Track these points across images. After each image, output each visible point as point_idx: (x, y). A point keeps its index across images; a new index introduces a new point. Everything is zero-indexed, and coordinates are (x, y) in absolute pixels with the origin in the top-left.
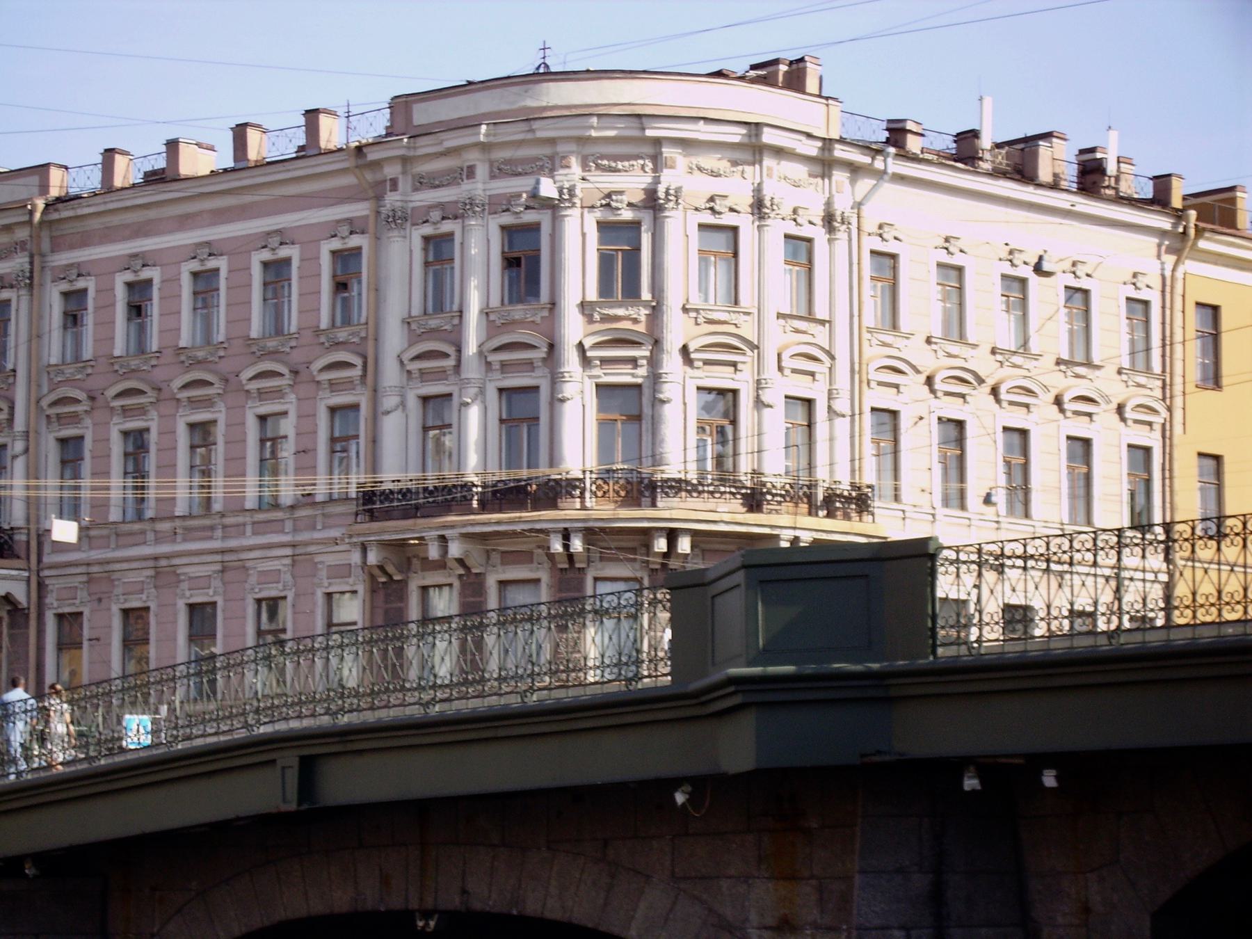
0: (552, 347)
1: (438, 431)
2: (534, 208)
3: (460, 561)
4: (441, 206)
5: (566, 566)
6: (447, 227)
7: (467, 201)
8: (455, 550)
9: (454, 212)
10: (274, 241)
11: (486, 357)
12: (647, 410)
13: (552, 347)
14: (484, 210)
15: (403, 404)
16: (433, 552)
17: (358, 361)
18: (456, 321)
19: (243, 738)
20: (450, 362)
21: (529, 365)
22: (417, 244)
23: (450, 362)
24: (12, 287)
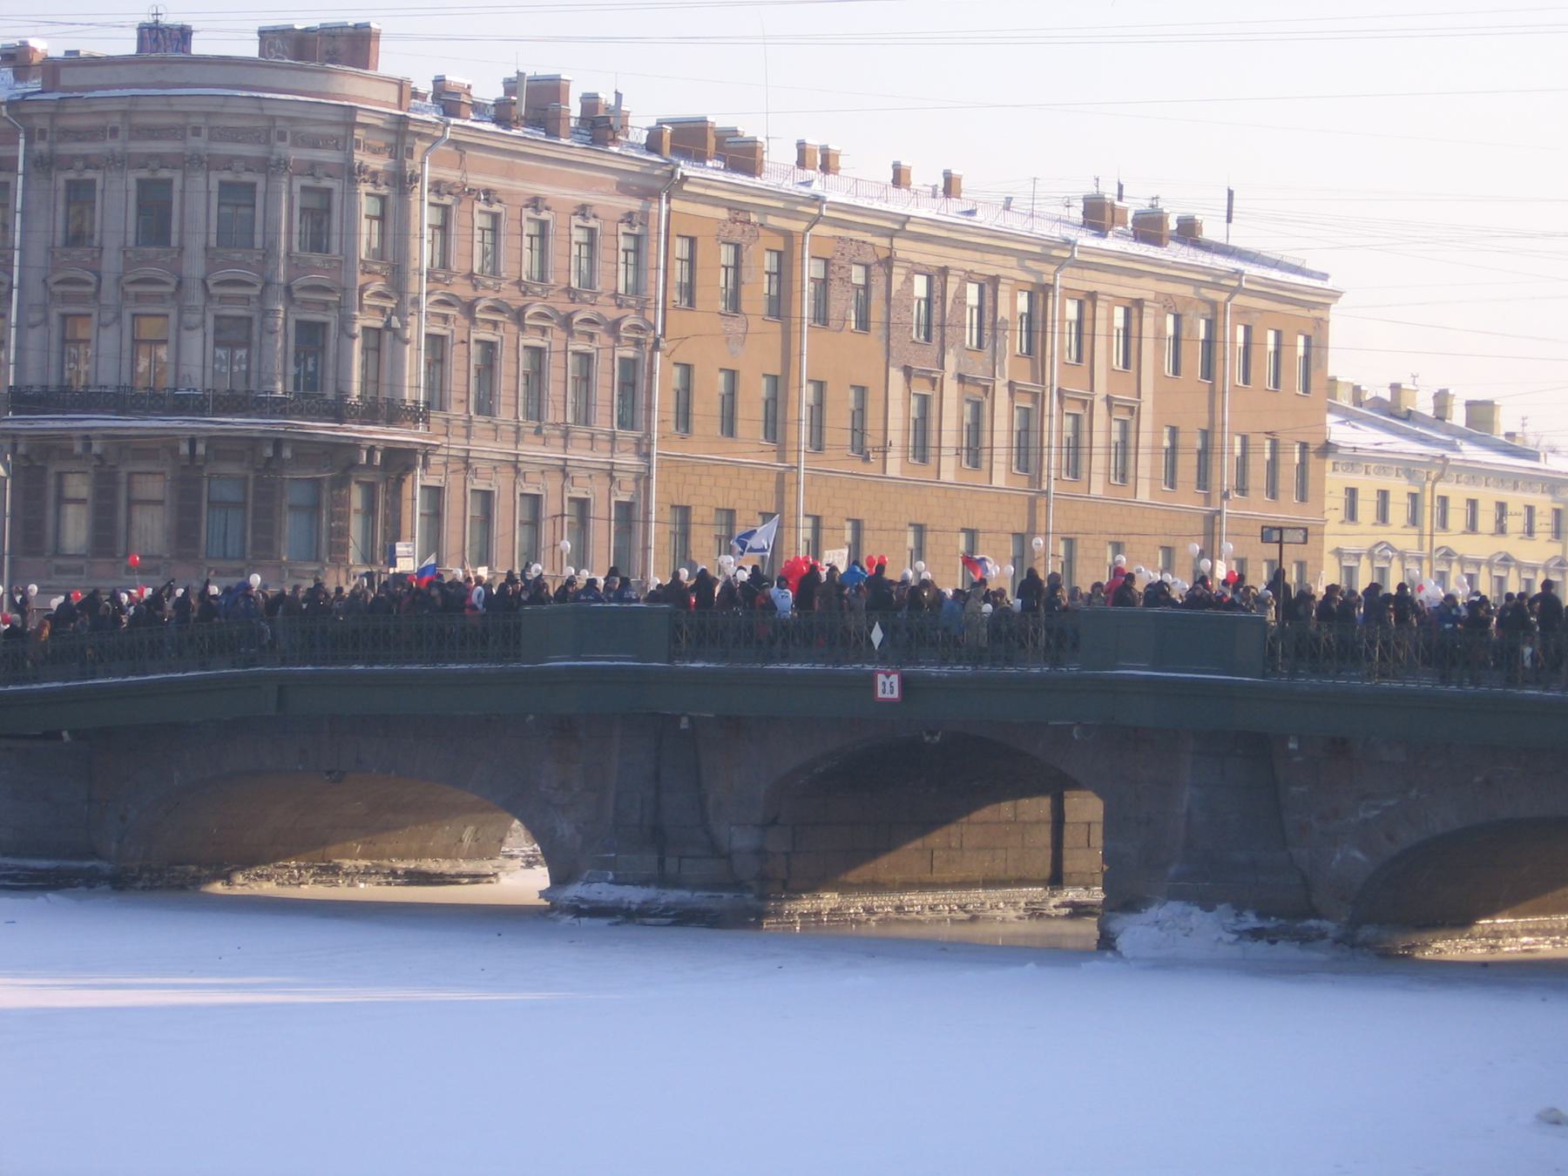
0: (180, 284)
1: (1202, 335)
2: (252, 171)
3: (99, 457)
4: (85, 157)
5: (187, 463)
6: (89, 174)
7: (110, 158)
8: (97, 448)
9: (187, 163)
10: (79, 165)
11: (123, 289)
12: (256, 338)
13: (180, 284)
14: (124, 164)
15: (46, 321)
16: (78, 448)
17: (92, 278)
18: (96, 255)
19: (1449, 586)
20: (91, 289)
21: (161, 298)
22: (133, 186)
23: (91, 289)
24: (98, 168)
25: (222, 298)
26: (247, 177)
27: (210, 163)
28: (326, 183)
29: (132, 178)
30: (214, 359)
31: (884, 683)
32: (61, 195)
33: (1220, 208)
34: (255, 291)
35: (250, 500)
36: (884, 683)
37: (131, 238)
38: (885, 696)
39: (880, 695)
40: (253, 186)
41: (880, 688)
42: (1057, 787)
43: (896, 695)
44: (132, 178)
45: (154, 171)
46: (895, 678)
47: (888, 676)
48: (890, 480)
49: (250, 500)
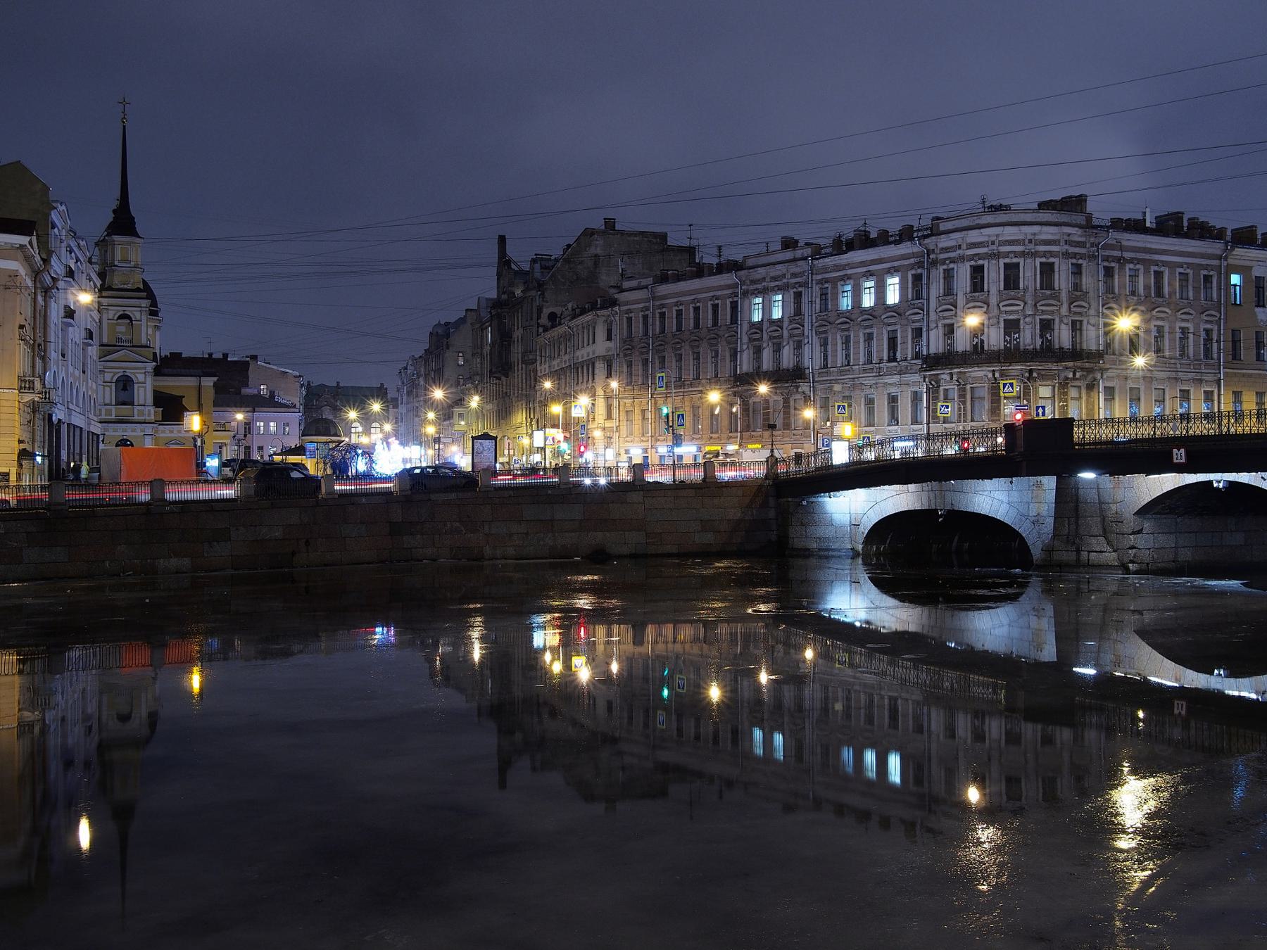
20: (953, 313)
25: (1006, 312)
26: (1015, 260)
27: (1034, 255)
28: (1080, 261)
29: (968, 265)
30: (1005, 341)
31: (1177, 454)
32: (942, 275)
33: (697, 228)
34: (1021, 308)
35: (1022, 395)
36: (1177, 454)
37: (968, 289)
38: (1178, 461)
39: (1175, 461)
40: (1018, 264)
41: (1175, 457)
42: (737, 623)
43: (1183, 461)
44: (968, 265)
45: (976, 261)
46: (1182, 451)
47: (1179, 451)
48: (1210, 371)
49: (1022, 395)
